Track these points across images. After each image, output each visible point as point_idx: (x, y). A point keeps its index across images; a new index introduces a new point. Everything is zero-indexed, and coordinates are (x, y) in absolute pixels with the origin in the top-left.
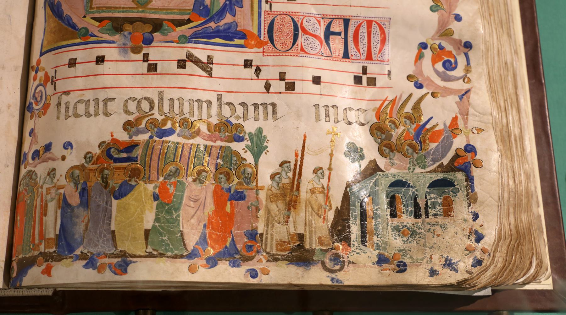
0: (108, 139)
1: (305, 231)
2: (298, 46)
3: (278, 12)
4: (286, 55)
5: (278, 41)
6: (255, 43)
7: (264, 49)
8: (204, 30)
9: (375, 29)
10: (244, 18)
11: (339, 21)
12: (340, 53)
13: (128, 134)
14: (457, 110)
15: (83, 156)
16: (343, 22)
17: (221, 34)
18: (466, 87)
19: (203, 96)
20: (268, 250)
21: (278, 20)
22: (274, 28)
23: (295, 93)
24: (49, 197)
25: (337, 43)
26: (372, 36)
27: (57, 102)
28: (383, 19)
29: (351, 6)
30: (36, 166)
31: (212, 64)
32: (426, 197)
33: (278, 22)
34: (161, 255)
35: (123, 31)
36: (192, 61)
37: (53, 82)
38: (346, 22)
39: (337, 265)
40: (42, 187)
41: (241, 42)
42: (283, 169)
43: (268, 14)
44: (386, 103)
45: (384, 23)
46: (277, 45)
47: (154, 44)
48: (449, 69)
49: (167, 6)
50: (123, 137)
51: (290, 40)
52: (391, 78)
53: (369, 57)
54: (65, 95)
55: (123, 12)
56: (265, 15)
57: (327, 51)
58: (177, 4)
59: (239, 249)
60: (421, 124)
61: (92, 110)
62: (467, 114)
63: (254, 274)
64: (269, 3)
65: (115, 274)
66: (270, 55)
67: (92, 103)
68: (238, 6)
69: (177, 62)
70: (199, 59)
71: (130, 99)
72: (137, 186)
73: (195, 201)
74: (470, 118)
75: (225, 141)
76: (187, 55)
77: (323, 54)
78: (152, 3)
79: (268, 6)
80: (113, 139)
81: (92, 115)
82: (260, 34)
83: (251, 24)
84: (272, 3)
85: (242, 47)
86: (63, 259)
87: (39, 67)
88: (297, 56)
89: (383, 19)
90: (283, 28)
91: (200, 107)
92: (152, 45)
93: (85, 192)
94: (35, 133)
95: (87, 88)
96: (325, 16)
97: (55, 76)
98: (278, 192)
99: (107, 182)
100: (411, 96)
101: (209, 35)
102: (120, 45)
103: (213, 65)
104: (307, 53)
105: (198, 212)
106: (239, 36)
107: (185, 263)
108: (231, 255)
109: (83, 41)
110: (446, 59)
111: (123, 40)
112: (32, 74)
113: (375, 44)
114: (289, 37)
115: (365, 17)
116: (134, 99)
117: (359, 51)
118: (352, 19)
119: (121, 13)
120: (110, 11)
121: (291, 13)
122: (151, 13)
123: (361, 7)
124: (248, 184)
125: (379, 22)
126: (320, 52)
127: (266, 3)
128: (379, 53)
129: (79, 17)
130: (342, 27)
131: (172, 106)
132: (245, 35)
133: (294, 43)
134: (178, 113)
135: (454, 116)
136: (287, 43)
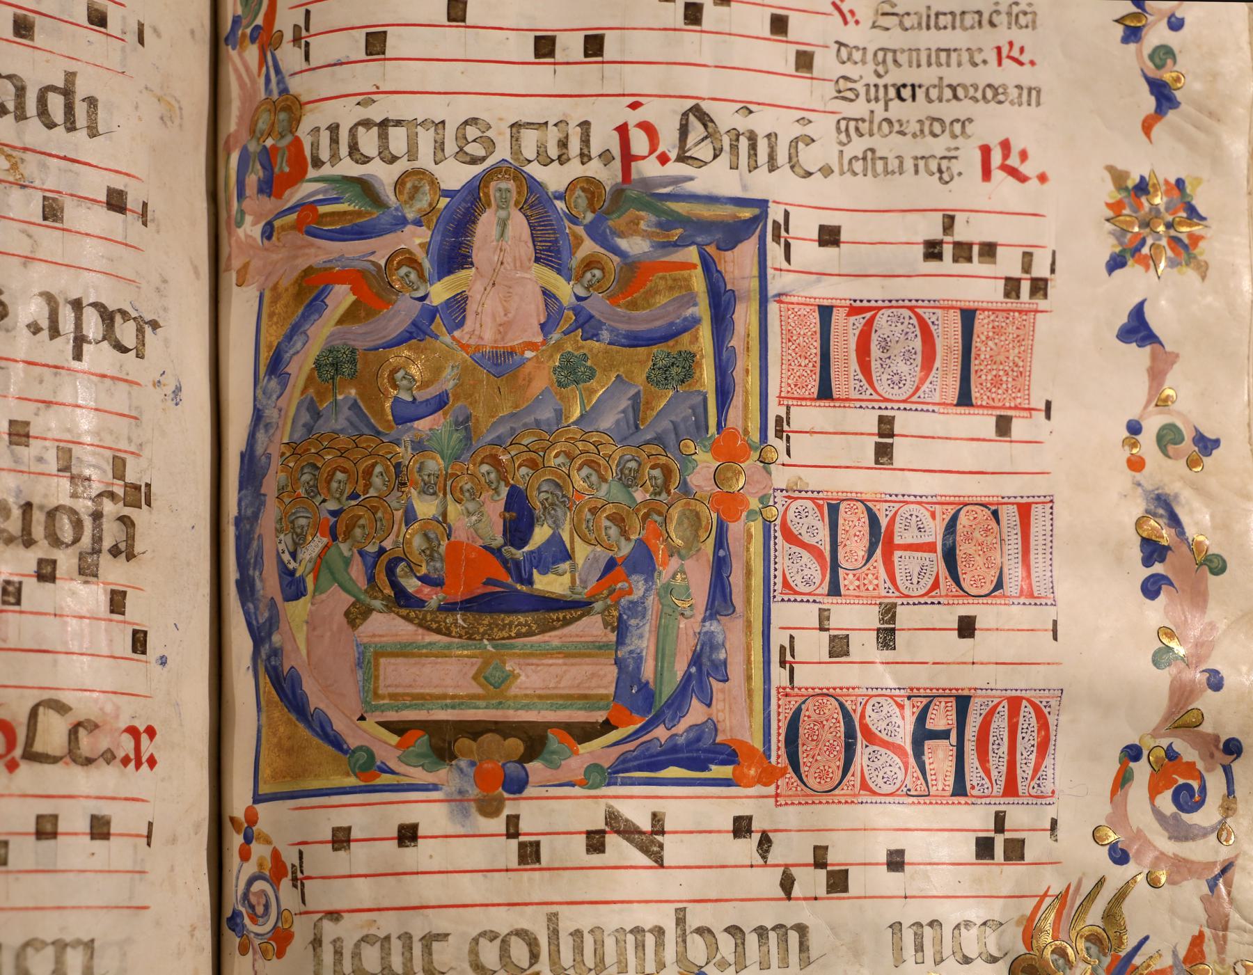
2: (854, 779)
4: (827, 803)
6: (756, 771)
7: (778, 787)
8: (642, 748)
9: (1027, 717)
11: (946, 702)
12: (947, 783)
14: (1203, 917)
16: (954, 704)
17: (681, 755)
18: (1224, 853)
19: (648, 917)
21: (809, 710)
23: (849, 898)
25: (940, 757)
26: (1019, 736)
27: (311, 937)
28: (1047, 691)
29: (973, 663)
31: (663, 833)
33: (809, 717)
35: (456, 757)
36: (618, 832)
37: (298, 882)
38: (963, 703)
41: (725, 771)
43: (787, 695)
44: (1048, 901)
47: (529, 791)
48: (1186, 807)
49: (554, 688)
51: (838, 763)
52: (1058, 838)
53: (1011, 789)
54: (331, 920)
55: (453, 707)
56: (779, 699)
57: (919, 782)
58: (577, 682)
60: (1123, 954)
62: (1225, 928)
64: (788, 666)
66: (793, 804)
67: (396, 946)
69: (584, 836)
70: (634, 825)
71: (483, 934)
74: (1231, 936)
77: (909, 790)
78: (519, 681)
79: (785, 673)
81: (553, 161)
85: (729, 785)
87: (254, 828)
88: (852, 802)
89: (1047, 691)
90: (821, 730)
91: (640, 946)
92: (526, 793)
95: (382, 906)
97: (301, 866)
100: (1102, 884)
101: (653, 759)
102: (452, 794)
104: (874, 793)
106: (721, 757)
109: (362, 784)
110: (1181, 781)
111: (458, 781)
112: (235, 841)
113: (1025, 755)
116: (494, 937)
117: (987, 772)
119: (449, 711)
120: (423, 705)
121: (838, 690)
122: (517, 709)
123: (997, 663)
126: (903, 788)
128: (1032, 779)
131: (579, 949)
132: (734, 754)
134: (592, 966)
135: (1197, 934)
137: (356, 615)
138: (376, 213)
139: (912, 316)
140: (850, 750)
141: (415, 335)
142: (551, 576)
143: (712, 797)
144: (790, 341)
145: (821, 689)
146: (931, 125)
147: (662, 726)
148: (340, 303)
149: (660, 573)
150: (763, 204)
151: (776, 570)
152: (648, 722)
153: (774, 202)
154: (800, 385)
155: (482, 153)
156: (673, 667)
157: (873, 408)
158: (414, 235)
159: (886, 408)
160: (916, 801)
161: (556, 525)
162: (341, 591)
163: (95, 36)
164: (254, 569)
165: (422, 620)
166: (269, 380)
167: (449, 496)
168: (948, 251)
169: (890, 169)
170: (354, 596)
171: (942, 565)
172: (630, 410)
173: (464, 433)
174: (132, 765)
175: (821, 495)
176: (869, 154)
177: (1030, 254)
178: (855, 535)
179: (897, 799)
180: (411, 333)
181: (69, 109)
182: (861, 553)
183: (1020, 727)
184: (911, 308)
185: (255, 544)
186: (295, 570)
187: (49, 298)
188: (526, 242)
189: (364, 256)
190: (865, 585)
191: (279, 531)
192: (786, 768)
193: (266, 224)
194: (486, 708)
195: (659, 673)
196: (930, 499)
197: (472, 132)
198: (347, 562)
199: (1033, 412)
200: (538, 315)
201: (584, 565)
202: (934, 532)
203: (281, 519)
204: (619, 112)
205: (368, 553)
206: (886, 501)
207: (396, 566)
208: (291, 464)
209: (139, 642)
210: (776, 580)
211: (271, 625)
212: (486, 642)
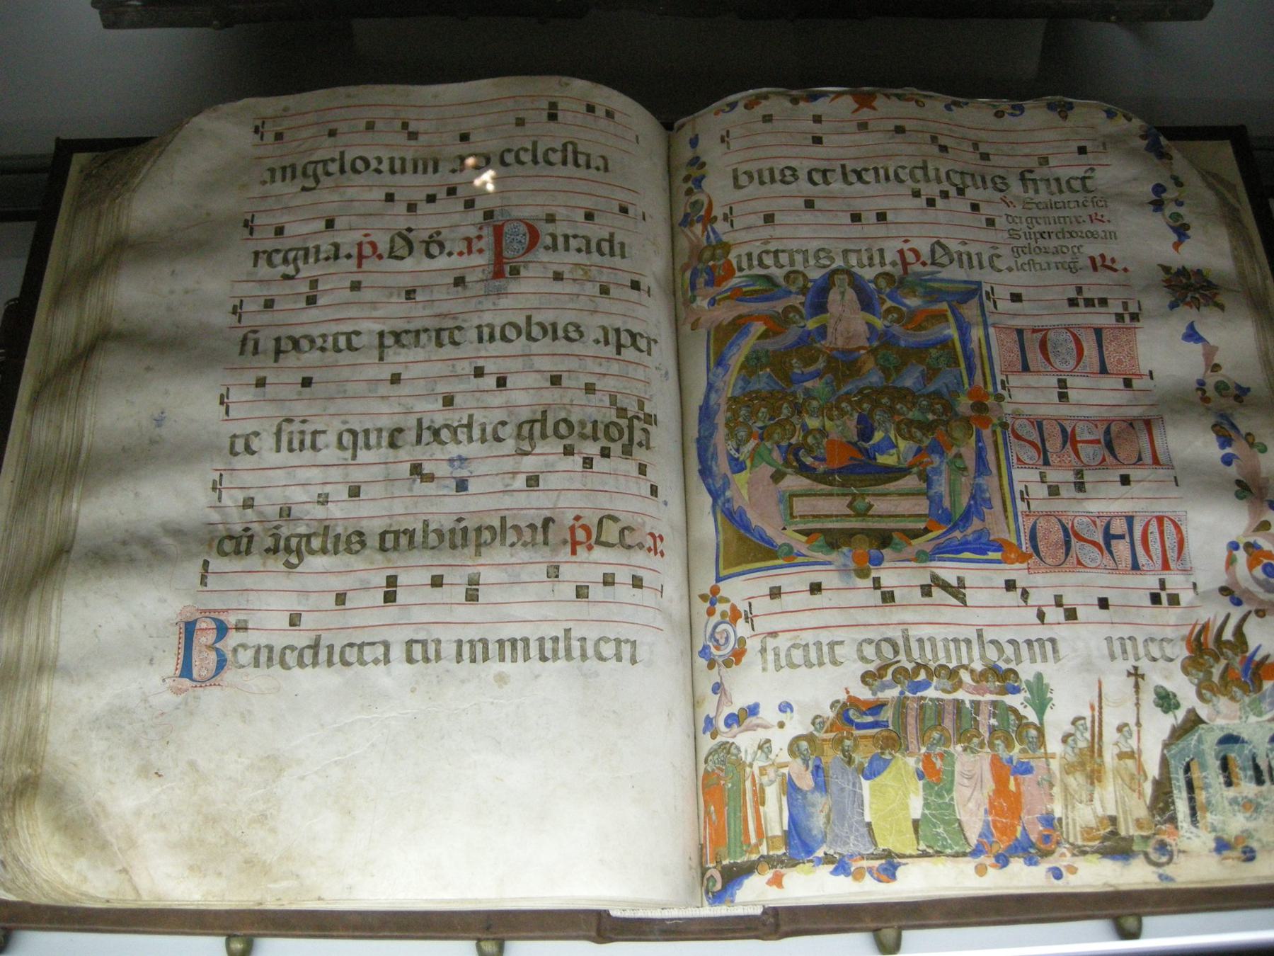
0: (843, 697)
1: (1118, 812)
13: (870, 689)
15: (810, 721)
20: (1071, 840)
21: (1041, 524)
24: (765, 779)
30: (735, 736)
31: (965, 588)
32: (1267, 756)
34: (939, 853)
36: (938, 586)
39: (1164, 855)
40: (751, 765)
41: (997, 555)
42: (1077, 729)
47: (885, 564)
50: (864, 694)
53: (1166, 566)
59: (1034, 840)
61: (813, 656)
63: (1057, 874)
65: (880, 881)
71: (864, 641)
72: (893, 762)
73: (970, 778)
75: (997, 694)
79: (1025, 504)
80: (850, 697)
86: (799, 863)
91: (958, 649)
93: (820, 771)
94: (724, 689)
98: (1075, 759)
99: (850, 757)
104: (1086, 567)
105: (975, 793)
107: (969, 862)
108: (1025, 850)
116: (870, 641)
117: (1150, 557)
124: (1034, 751)
130: (1125, 527)
131: (922, 648)
133: (1067, 555)
137: (777, 477)
138: (776, 289)
150: (979, 283)
155: (829, 263)
161: (887, 431)
163: (622, 217)
168: (1081, 302)
174: (652, 552)
181: (612, 248)
185: (711, 449)
187: (604, 329)
191: (727, 440)
195: (953, 503)
197: (822, 254)
198: (770, 451)
202: (1099, 434)
204: (899, 245)
209: (654, 491)
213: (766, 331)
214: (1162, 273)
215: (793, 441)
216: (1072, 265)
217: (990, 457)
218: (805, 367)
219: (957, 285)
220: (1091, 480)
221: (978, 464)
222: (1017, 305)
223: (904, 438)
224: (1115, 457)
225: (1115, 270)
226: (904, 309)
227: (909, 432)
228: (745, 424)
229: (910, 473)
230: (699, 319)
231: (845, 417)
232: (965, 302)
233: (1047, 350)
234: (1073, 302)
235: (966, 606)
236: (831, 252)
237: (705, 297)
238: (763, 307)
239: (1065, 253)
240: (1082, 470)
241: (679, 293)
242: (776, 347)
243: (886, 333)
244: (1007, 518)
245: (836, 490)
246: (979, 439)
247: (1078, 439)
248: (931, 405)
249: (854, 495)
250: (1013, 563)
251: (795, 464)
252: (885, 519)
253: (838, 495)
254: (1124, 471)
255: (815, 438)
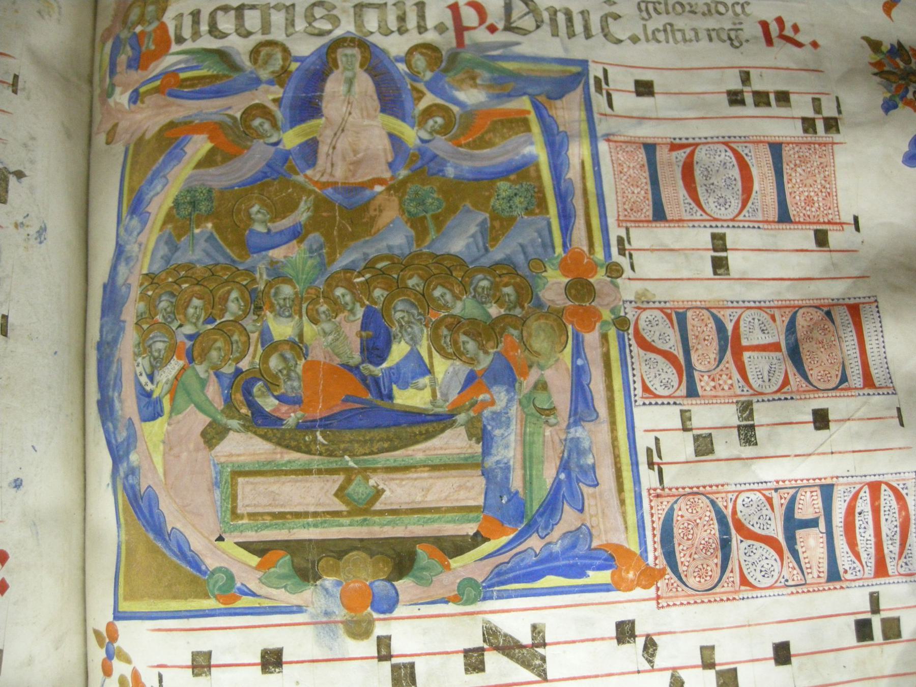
3: (680, 490)
4: (710, 601)
5: (687, 564)
6: (635, 574)
7: (658, 589)
8: (516, 559)
10: (603, 513)
11: (812, 492)
12: (821, 570)
16: (819, 493)
21: (683, 511)
22: (675, 530)
26: (883, 519)
31: (544, 645)
33: (682, 516)
35: (320, 578)
36: (497, 648)
38: (827, 491)
41: (604, 577)
43: (658, 496)
45: (904, 484)
46: (686, 576)
47: (399, 611)
49: (420, 503)
51: (715, 561)
53: (881, 569)
56: (651, 501)
64: (656, 467)
68: (588, 482)
69: (462, 655)
76: (484, 635)
77: (787, 581)
78: (383, 496)
79: (654, 475)
81: (392, 32)
82: (646, 551)
83: (622, 527)
84: (662, 466)
85: (608, 590)
88: (734, 599)
92: (396, 613)
96: (781, 483)
101: (529, 570)
102: (317, 615)
103: (547, 647)
104: (754, 587)
106: (598, 562)
109: (222, 606)
111: (323, 601)
114: (712, 551)
115: (865, 476)
117: (857, 556)
118: (838, 485)
119: (312, 529)
121: (708, 488)
125: (894, 484)
127: (649, 468)
128: (900, 558)
129: (207, 538)
136: (709, 568)
138: (235, 75)
139: (727, 149)
140: (725, 545)
141: (269, 174)
142: (411, 391)
143: (592, 604)
144: (621, 172)
145: (691, 488)
146: (716, 6)
147: (535, 535)
148: (199, 150)
149: (521, 383)
150: (584, 63)
151: (634, 375)
152: (521, 532)
153: (594, 62)
154: (635, 210)
156: (542, 474)
157: (705, 227)
158: (267, 92)
159: (717, 227)
160: (795, 591)
161: (414, 341)
162: (197, 411)
164: (114, 391)
165: (280, 439)
166: (131, 219)
167: (305, 318)
168: (749, 98)
169: (688, 37)
170: (209, 415)
171: (789, 363)
172: (479, 235)
173: (318, 259)
175: (668, 305)
176: (668, 27)
177: (819, 100)
178: (705, 340)
179: (776, 591)
180: (265, 173)
182: (713, 356)
183: (882, 509)
184: (726, 144)
185: (114, 368)
186: (152, 392)
188: (371, 96)
189: (221, 111)
190: (720, 385)
191: (137, 355)
192: (664, 569)
193: (133, 92)
194: (350, 525)
195: (528, 482)
196: (768, 304)
198: (203, 383)
199: (845, 226)
200: (386, 155)
201: (444, 378)
202: (777, 334)
203: (139, 344)
205: (223, 374)
206: (728, 308)
207: (253, 385)
208: (150, 293)
210: (636, 385)
211: (128, 445)
212: (347, 458)
213: (211, 153)
214: (868, 50)
215: (244, 365)
216: (733, 35)
217: (597, 385)
218: (273, 220)
219: (546, 67)
220: (765, 421)
221: (574, 401)
222: (645, 102)
223: (446, 355)
224: (805, 376)
225: (799, 45)
226: (455, 109)
227: (455, 343)
228: (165, 326)
229: (452, 425)
230: (116, 125)
231: (341, 316)
232: (560, 97)
233: (694, 181)
234: (735, 99)
235: (545, 680)
236: (334, 7)
237: (125, 87)
238: (210, 107)
239: (721, 14)
240: (750, 403)
241: (96, 79)
242: (225, 183)
243: (421, 153)
244: (622, 502)
245: (316, 461)
246: (578, 351)
247: (744, 343)
248: (495, 286)
249: (348, 470)
250: (630, 589)
251: (244, 410)
252: (404, 518)
253: (320, 472)
254: (819, 403)
255: (283, 358)
